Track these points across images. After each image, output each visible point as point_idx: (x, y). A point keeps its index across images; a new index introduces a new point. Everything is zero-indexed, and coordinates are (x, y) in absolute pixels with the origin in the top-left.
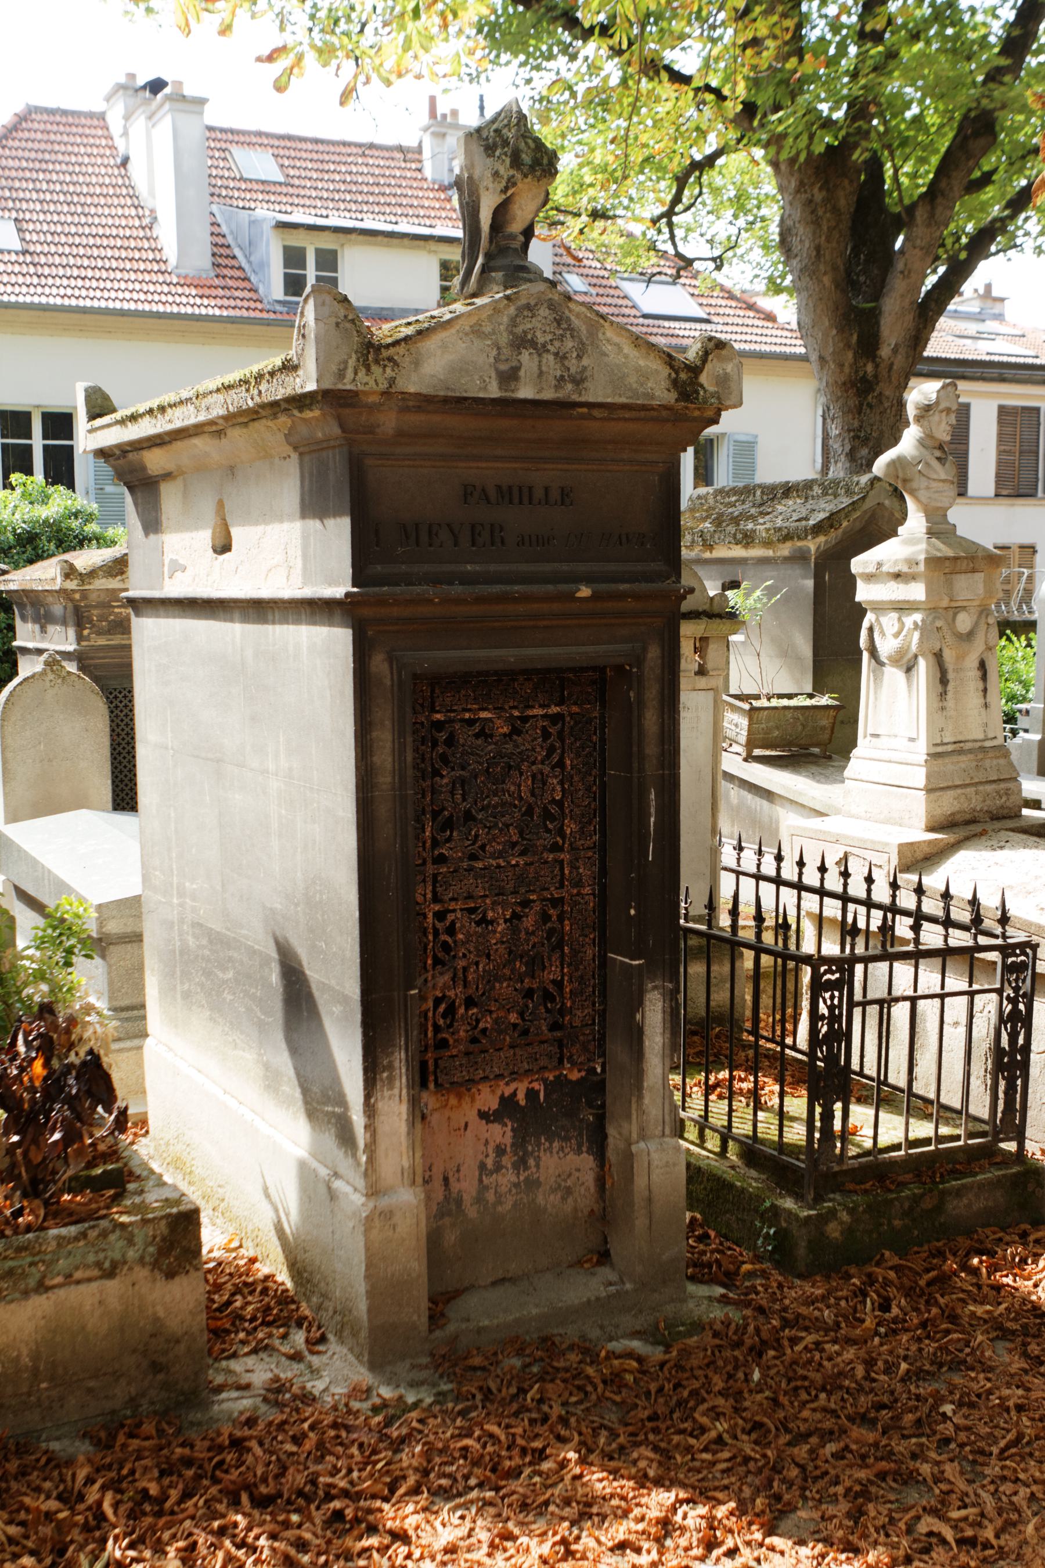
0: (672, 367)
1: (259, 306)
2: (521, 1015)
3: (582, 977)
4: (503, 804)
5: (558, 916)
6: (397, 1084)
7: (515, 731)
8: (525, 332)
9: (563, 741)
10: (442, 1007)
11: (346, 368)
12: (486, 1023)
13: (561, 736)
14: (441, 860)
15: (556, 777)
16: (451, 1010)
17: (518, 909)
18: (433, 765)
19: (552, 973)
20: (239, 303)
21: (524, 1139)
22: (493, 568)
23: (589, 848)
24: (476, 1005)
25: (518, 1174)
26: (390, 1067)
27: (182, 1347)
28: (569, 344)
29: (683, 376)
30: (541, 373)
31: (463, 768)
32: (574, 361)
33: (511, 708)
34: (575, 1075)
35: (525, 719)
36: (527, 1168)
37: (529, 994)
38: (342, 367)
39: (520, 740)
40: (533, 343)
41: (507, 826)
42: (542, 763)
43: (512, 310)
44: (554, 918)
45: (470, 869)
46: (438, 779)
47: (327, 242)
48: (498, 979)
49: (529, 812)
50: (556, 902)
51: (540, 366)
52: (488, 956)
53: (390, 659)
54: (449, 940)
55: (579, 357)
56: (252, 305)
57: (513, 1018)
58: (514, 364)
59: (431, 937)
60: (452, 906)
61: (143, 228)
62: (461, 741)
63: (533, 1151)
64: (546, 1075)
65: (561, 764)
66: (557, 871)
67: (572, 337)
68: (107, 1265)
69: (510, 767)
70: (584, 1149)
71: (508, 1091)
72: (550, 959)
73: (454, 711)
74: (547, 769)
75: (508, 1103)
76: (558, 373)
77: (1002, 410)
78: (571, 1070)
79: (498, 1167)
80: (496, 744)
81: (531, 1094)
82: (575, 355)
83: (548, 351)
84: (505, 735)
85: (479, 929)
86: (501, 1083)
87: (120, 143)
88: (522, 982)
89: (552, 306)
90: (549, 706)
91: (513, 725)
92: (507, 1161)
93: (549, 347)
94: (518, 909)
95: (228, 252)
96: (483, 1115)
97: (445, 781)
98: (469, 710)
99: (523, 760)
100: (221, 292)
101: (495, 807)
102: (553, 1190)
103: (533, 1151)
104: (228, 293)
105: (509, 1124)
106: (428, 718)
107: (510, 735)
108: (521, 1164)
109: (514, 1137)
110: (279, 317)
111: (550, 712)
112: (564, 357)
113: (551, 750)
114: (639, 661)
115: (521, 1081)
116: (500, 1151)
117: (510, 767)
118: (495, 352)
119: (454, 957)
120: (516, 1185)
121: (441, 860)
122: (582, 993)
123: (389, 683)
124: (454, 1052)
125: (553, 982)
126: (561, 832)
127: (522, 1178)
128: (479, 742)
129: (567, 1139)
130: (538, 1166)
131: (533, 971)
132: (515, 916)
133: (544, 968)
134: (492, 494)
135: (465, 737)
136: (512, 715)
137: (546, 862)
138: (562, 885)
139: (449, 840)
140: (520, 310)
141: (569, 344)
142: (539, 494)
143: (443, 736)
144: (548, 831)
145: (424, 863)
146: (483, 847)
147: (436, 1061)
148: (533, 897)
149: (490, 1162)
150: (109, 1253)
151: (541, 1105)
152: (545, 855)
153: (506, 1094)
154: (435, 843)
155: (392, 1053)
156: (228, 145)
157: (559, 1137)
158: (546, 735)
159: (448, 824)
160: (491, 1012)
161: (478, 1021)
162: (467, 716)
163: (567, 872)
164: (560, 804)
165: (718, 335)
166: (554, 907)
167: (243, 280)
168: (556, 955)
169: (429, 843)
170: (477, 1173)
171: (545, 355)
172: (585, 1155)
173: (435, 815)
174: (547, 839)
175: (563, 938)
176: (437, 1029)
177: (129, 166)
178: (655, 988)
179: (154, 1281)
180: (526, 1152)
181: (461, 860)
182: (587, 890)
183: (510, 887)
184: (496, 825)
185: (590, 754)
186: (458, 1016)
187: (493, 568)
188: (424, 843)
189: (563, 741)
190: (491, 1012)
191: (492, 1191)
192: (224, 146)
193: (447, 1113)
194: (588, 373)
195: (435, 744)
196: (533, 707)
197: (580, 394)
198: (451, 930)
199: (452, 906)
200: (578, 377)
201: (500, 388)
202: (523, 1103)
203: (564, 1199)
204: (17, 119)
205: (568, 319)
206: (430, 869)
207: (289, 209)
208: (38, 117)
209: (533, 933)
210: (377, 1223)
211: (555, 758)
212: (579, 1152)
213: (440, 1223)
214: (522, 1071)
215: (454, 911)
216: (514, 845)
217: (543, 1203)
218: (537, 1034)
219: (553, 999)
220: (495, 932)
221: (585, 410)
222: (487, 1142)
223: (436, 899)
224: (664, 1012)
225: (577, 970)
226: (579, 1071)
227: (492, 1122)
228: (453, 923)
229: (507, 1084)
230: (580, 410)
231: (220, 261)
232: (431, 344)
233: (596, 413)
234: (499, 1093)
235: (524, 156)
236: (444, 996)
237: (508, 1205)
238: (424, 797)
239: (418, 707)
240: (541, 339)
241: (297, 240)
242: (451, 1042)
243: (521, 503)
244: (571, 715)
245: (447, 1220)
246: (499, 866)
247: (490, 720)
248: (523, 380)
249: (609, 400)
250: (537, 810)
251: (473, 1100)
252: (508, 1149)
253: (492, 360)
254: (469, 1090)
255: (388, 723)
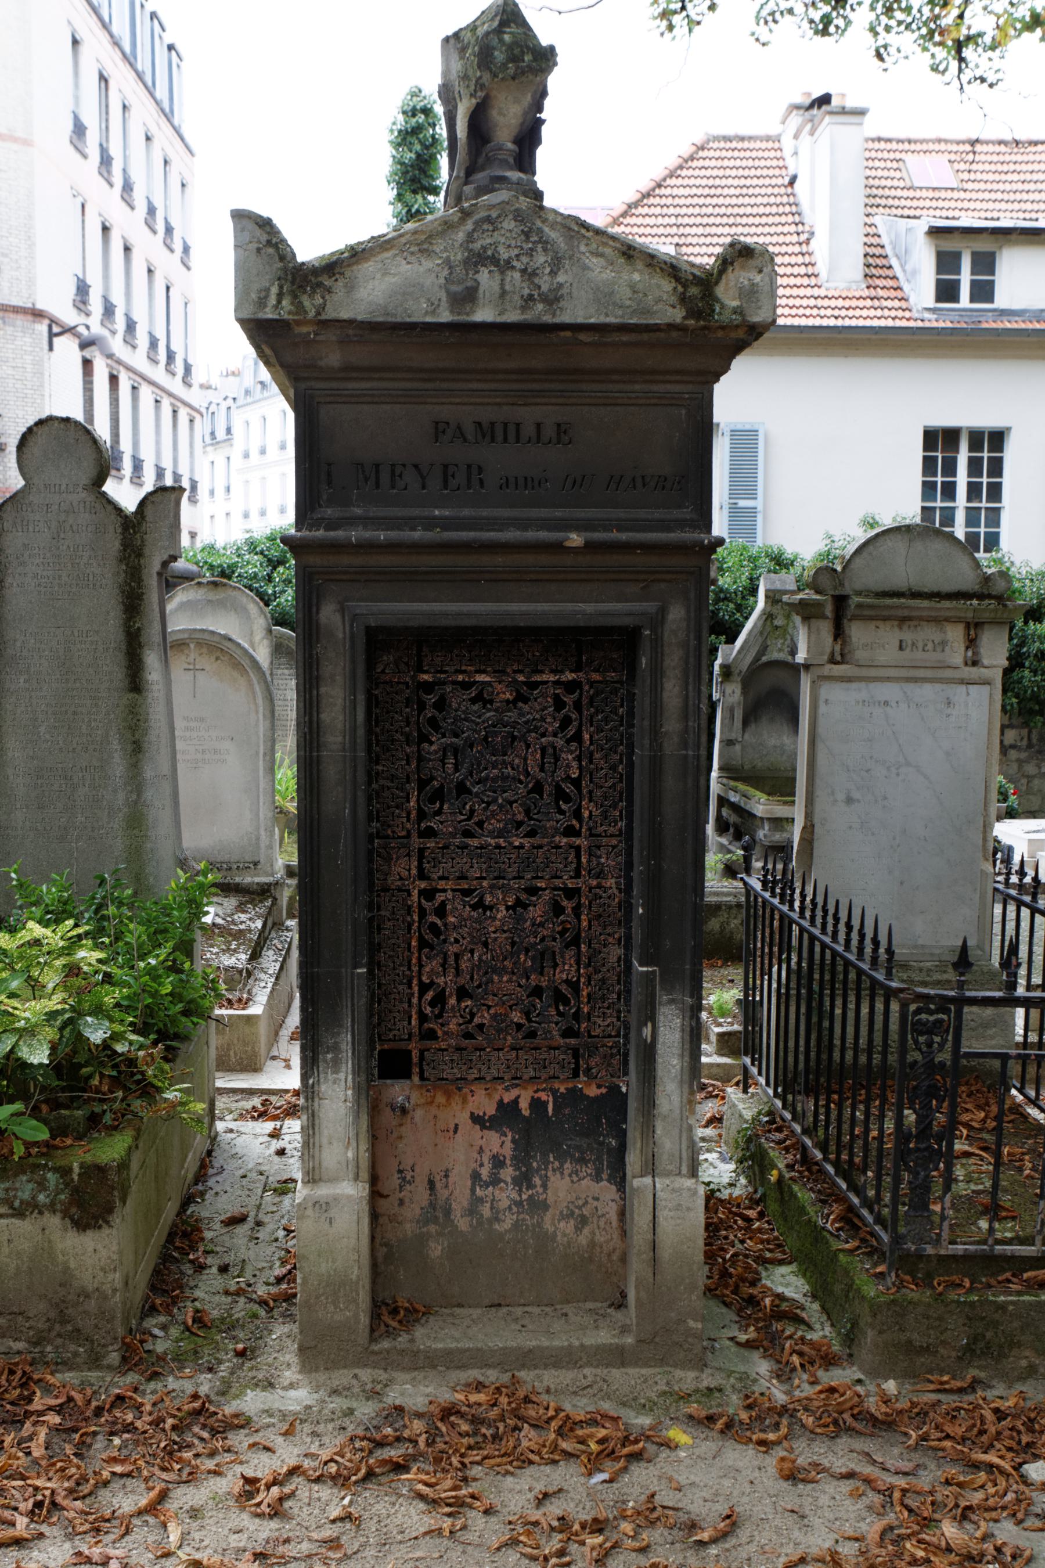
0: (677, 279)
1: (907, 314)
2: (527, 1014)
3: (603, 981)
4: (505, 778)
5: (573, 909)
6: (344, 1069)
7: (521, 698)
8: (484, 248)
9: (580, 712)
10: (430, 995)
11: (267, 297)
12: (484, 1017)
13: (578, 706)
14: (430, 833)
15: (572, 752)
16: (440, 999)
17: (523, 896)
18: (419, 730)
19: (566, 971)
20: (886, 313)
21: (527, 1153)
22: (466, 512)
23: (612, 836)
24: (471, 997)
25: (520, 1191)
26: (336, 1048)
27: (92, 1305)
28: (541, 259)
29: (694, 291)
30: (503, 293)
31: (456, 736)
32: (546, 278)
33: (515, 672)
34: (593, 1091)
35: (534, 685)
36: (530, 1186)
37: (537, 992)
38: (263, 294)
39: (526, 708)
40: (494, 260)
41: (511, 803)
42: (555, 735)
43: (469, 226)
44: (569, 911)
45: (464, 847)
46: (426, 745)
47: (983, 245)
48: (501, 971)
49: (538, 788)
50: (571, 893)
51: (502, 285)
52: (485, 944)
53: (342, 611)
54: (439, 922)
55: (553, 273)
56: (900, 314)
57: (516, 1017)
58: (469, 284)
59: (416, 918)
60: (442, 885)
61: (800, 244)
62: (454, 705)
63: (539, 1169)
64: (556, 1086)
65: (577, 737)
66: (571, 857)
67: (545, 250)
68: (17, 1204)
69: (514, 738)
70: (605, 1176)
71: (508, 1097)
72: (563, 957)
73: (445, 672)
74: (560, 742)
75: (507, 1113)
76: (526, 292)
77: (992, 301)
78: (588, 1084)
79: (495, 1181)
80: (496, 710)
81: (537, 1105)
82: (548, 270)
83: (513, 268)
84: (508, 702)
85: (475, 914)
86: (500, 1088)
87: (790, 162)
88: (528, 978)
89: (519, 216)
90: (562, 672)
91: (518, 691)
92: (508, 1173)
93: (515, 263)
94: (523, 896)
95: (884, 262)
96: (477, 1119)
97: (433, 748)
98: (464, 672)
99: (529, 731)
100: (869, 303)
101: (495, 780)
102: (563, 1217)
103: (539, 1169)
104: (876, 303)
105: (510, 1135)
106: (413, 678)
107: (514, 702)
108: (523, 1180)
109: (515, 1150)
110: (927, 324)
111: (563, 678)
112: (534, 274)
113: (566, 722)
114: (658, 620)
115: (525, 1088)
116: (498, 1162)
117: (514, 738)
118: (446, 272)
119: (445, 941)
120: (519, 1204)
121: (430, 833)
122: (603, 998)
123: (341, 636)
124: (443, 1046)
125: (567, 982)
126: (577, 814)
127: (524, 1197)
128: (475, 707)
129: (582, 1161)
130: (545, 1186)
131: (542, 967)
132: (518, 903)
133: (555, 966)
134: (469, 430)
135: (460, 701)
136: (515, 681)
137: (558, 847)
138: (578, 875)
139: (439, 812)
140: (478, 224)
141: (541, 259)
142: (528, 430)
143: (432, 699)
144: (562, 812)
145: (408, 836)
146: (480, 824)
147: (422, 1053)
148: (541, 884)
149: (485, 1173)
150: (19, 1194)
151: (549, 1118)
152: (557, 839)
153: (506, 1101)
154: (422, 815)
155: (339, 1034)
156: (903, 156)
157: (572, 1157)
158: (559, 704)
159: (438, 795)
160: (489, 1007)
161: (473, 1015)
162: (460, 678)
163: (584, 860)
164: (577, 783)
165: (742, 239)
166: (569, 898)
167: (895, 289)
168: (570, 953)
169: (414, 814)
170: (469, 1183)
171: (509, 273)
172: (604, 1183)
173: (422, 784)
174: (564, 822)
175: (579, 934)
176: (423, 1018)
177: (796, 185)
178: (672, 1001)
179: (66, 1230)
180: (529, 1167)
181: (453, 835)
182: (611, 882)
183: (512, 872)
184: (495, 800)
185: (615, 729)
186: (449, 1006)
187: (466, 512)
188: (409, 814)
189: (580, 712)
190: (489, 1007)
191: (488, 1205)
192: (898, 156)
193: (434, 1110)
194: (564, 291)
195: (422, 706)
196: (542, 672)
197: (554, 315)
198: (441, 911)
199: (442, 885)
200: (551, 297)
201: (452, 312)
202: (526, 1113)
203: (578, 1229)
204: (694, 148)
205: (540, 231)
206: (416, 842)
207: (957, 214)
208: (716, 145)
209: (541, 925)
210: (309, 1212)
211: (571, 731)
212: (597, 1178)
213: (425, 1230)
214: (526, 1077)
215: (444, 891)
216: (519, 824)
217: (551, 1229)
218: (546, 1039)
219: (566, 1002)
220: (494, 919)
221: (568, 334)
222: (481, 1151)
223: (422, 875)
224: (683, 1031)
225: (597, 971)
226: (599, 1087)
227: (489, 1128)
228: (443, 904)
229: (507, 1089)
230: (562, 334)
231: (874, 271)
232: (369, 267)
233: (583, 337)
234: (497, 1097)
235: (496, 53)
236: (432, 983)
237: (507, 1224)
238: (408, 763)
239: (402, 666)
240: (504, 254)
241: (950, 245)
242: (440, 1033)
243: (505, 440)
244: (592, 684)
245: (433, 1228)
246: (498, 847)
247: (489, 684)
248: (481, 301)
249: (592, 321)
250: (547, 789)
251: (465, 1101)
252: (508, 1162)
253: (442, 281)
254: (460, 1089)
255: (339, 679)
